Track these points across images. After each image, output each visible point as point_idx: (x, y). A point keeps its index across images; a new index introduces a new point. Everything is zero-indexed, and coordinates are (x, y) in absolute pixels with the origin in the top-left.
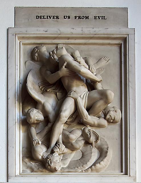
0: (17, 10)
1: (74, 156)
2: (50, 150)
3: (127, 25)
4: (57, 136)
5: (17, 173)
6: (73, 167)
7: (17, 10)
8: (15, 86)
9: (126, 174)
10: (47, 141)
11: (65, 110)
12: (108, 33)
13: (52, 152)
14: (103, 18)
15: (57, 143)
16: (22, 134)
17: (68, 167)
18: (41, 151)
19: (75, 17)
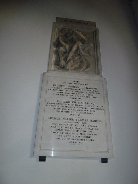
0: (107, 162)
1: (76, 66)
2: (66, 62)
3: (95, 27)
4: (70, 57)
5: (52, 69)
6: (76, 69)
7: (107, 162)
8: (55, 39)
9: (98, 74)
10: (65, 59)
11: (74, 48)
12: (35, 147)
13: (68, 63)
14: (87, 24)
15: (70, 60)
16: (55, 56)
17: (74, 69)
18: (63, 63)
19: (78, 22)
